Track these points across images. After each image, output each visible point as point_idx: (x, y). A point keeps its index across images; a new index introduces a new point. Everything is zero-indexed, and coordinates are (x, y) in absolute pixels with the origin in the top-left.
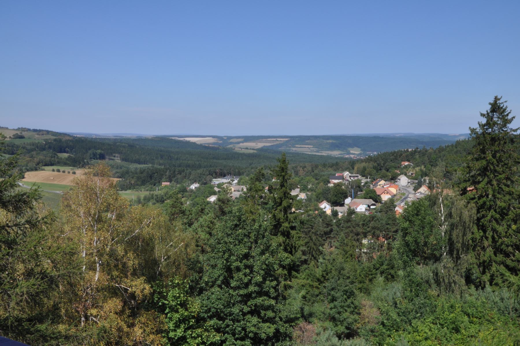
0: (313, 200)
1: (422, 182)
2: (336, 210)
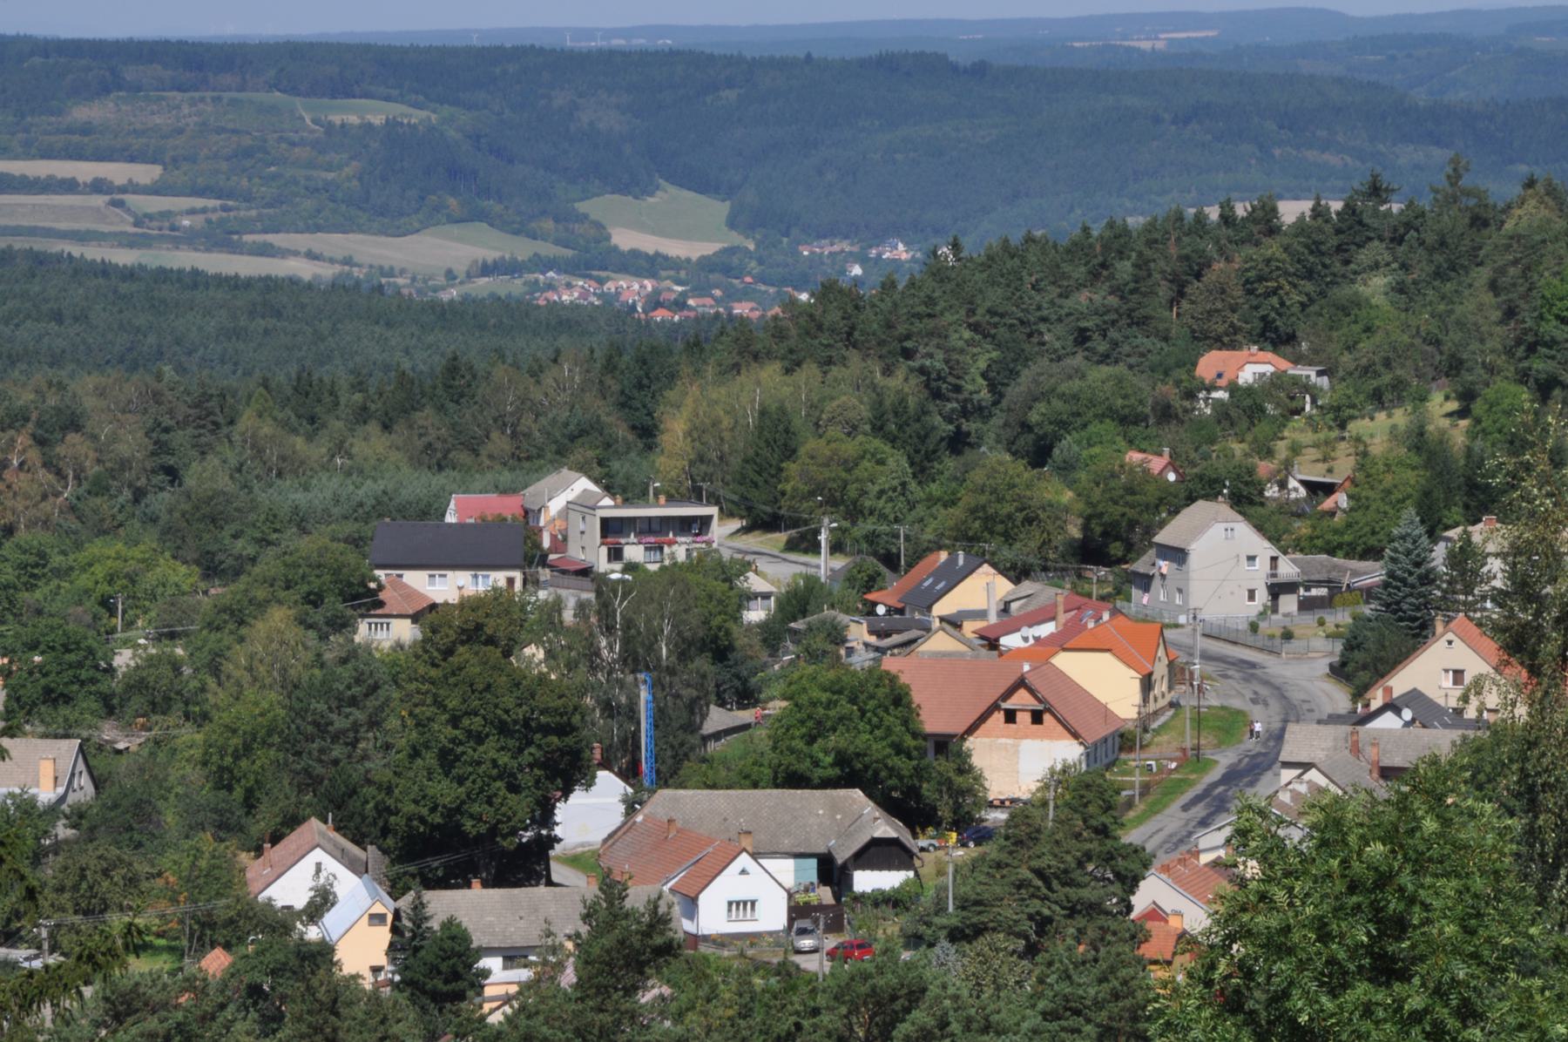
0: (170, 817)
1: (1428, 579)
2: (449, 924)
